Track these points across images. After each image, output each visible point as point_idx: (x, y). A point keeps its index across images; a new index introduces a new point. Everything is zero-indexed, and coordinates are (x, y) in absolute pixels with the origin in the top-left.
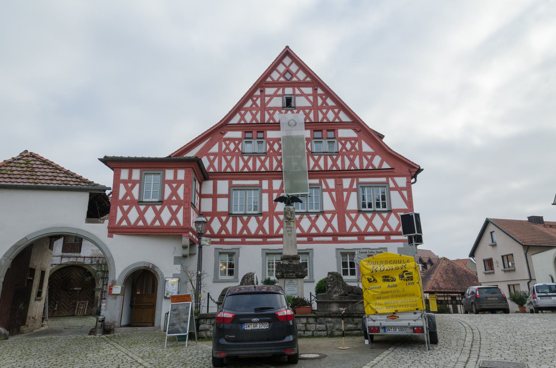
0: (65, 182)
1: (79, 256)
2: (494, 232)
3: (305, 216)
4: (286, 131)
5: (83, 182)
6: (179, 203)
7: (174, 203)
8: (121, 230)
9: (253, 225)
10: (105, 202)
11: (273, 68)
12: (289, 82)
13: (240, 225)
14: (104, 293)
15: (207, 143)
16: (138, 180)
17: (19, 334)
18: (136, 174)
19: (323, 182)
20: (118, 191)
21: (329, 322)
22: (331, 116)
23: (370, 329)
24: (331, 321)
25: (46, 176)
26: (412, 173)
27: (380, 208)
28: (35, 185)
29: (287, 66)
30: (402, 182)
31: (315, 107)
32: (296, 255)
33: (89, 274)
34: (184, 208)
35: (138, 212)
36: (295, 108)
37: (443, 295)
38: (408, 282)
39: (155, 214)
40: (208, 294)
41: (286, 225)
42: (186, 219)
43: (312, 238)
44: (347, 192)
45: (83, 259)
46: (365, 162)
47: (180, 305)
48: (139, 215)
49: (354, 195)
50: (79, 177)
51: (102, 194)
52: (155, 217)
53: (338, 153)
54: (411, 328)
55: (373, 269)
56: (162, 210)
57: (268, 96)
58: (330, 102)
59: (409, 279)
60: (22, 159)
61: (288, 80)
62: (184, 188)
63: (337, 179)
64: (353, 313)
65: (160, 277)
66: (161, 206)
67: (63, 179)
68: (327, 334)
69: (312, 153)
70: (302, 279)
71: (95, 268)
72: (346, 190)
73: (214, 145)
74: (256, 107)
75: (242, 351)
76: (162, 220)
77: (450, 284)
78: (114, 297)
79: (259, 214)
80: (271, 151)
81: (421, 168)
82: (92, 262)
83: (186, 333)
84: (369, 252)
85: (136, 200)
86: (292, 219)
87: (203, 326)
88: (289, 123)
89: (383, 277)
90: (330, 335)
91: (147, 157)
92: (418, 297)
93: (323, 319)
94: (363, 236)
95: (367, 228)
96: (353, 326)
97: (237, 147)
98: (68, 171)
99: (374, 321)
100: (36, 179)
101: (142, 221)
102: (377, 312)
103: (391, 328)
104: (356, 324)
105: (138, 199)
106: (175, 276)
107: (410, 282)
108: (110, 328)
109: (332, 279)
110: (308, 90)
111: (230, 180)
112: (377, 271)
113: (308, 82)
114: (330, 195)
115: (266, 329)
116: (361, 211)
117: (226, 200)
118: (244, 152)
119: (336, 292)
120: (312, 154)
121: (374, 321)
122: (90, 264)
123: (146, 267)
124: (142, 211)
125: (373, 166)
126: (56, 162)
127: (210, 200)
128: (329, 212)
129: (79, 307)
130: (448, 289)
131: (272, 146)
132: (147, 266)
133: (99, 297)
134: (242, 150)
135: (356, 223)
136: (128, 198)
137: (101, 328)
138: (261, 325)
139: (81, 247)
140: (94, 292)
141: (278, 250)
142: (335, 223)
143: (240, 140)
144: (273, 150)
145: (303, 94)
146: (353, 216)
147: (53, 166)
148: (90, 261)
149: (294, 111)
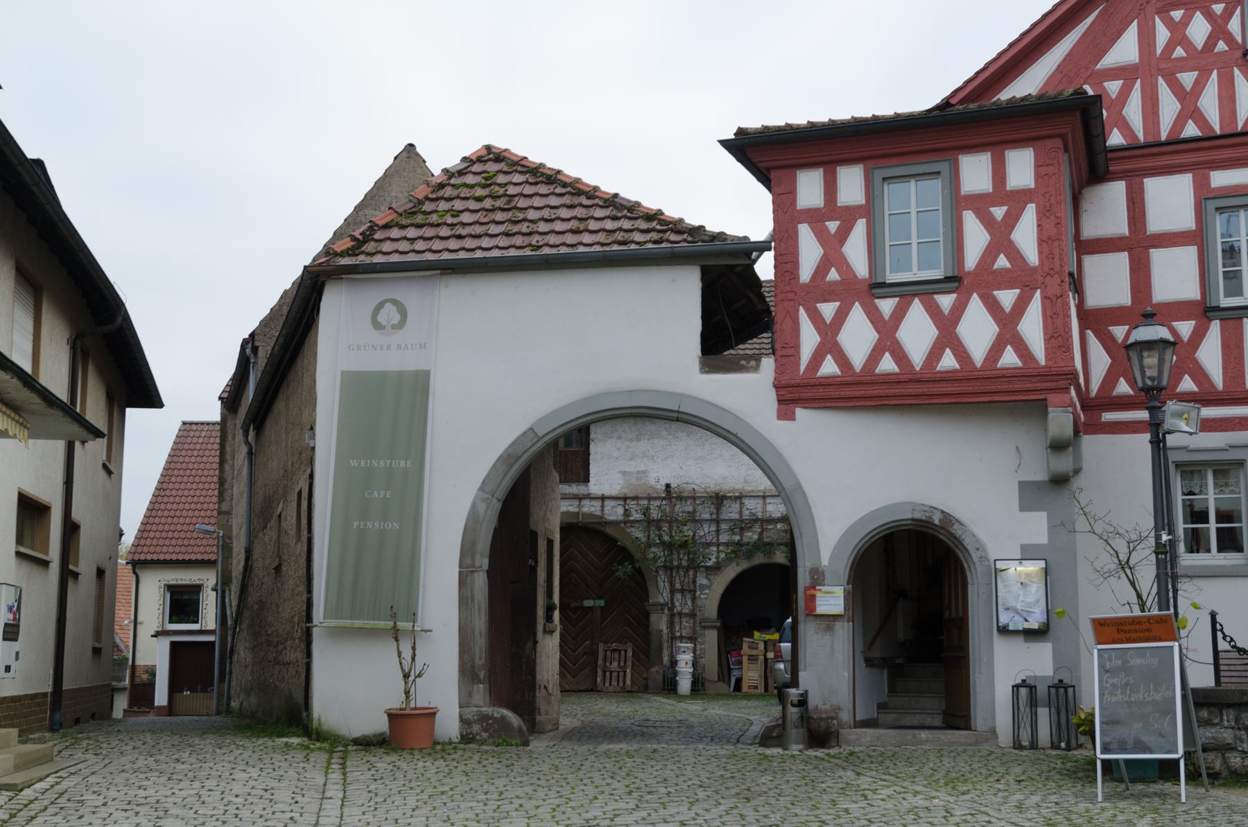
0: (619, 236)
1: (586, 493)
5: (672, 230)
6: (1023, 278)
7: (1005, 280)
8: (820, 392)
10: (751, 295)
14: (677, 619)
17: (534, 732)
25: (556, 222)
28: (534, 253)
33: (624, 554)
34: (1045, 298)
39: (938, 328)
40: (1213, 616)
45: (598, 504)
47: (1131, 652)
50: (655, 214)
51: (738, 269)
52: (937, 339)
56: (959, 309)
60: (470, 172)
62: (1039, 219)
65: (975, 556)
66: (955, 295)
67: (609, 225)
71: (638, 533)
73: (1119, 34)
76: (963, 346)
82: (627, 512)
85: (861, 280)
87: (1208, 734)
91: (782, 123)
98: (616, 195)
100: (530, 234)
105: (867, 276)
106: (1027, 554)
108: (828, 728)
111: (1201, 171)
117: (1189, 254)
122: (621, 522)
123: (922, 521)
126: (572, 170)
127: (1120, 262)
129: (607, 664)
132: (924, 518)
133: (665, 631)
136: (833, 275)
137: (802, 726)
139: (589, 464)
140: (647, 615)
147: (564, 185)
148: (620, 511)
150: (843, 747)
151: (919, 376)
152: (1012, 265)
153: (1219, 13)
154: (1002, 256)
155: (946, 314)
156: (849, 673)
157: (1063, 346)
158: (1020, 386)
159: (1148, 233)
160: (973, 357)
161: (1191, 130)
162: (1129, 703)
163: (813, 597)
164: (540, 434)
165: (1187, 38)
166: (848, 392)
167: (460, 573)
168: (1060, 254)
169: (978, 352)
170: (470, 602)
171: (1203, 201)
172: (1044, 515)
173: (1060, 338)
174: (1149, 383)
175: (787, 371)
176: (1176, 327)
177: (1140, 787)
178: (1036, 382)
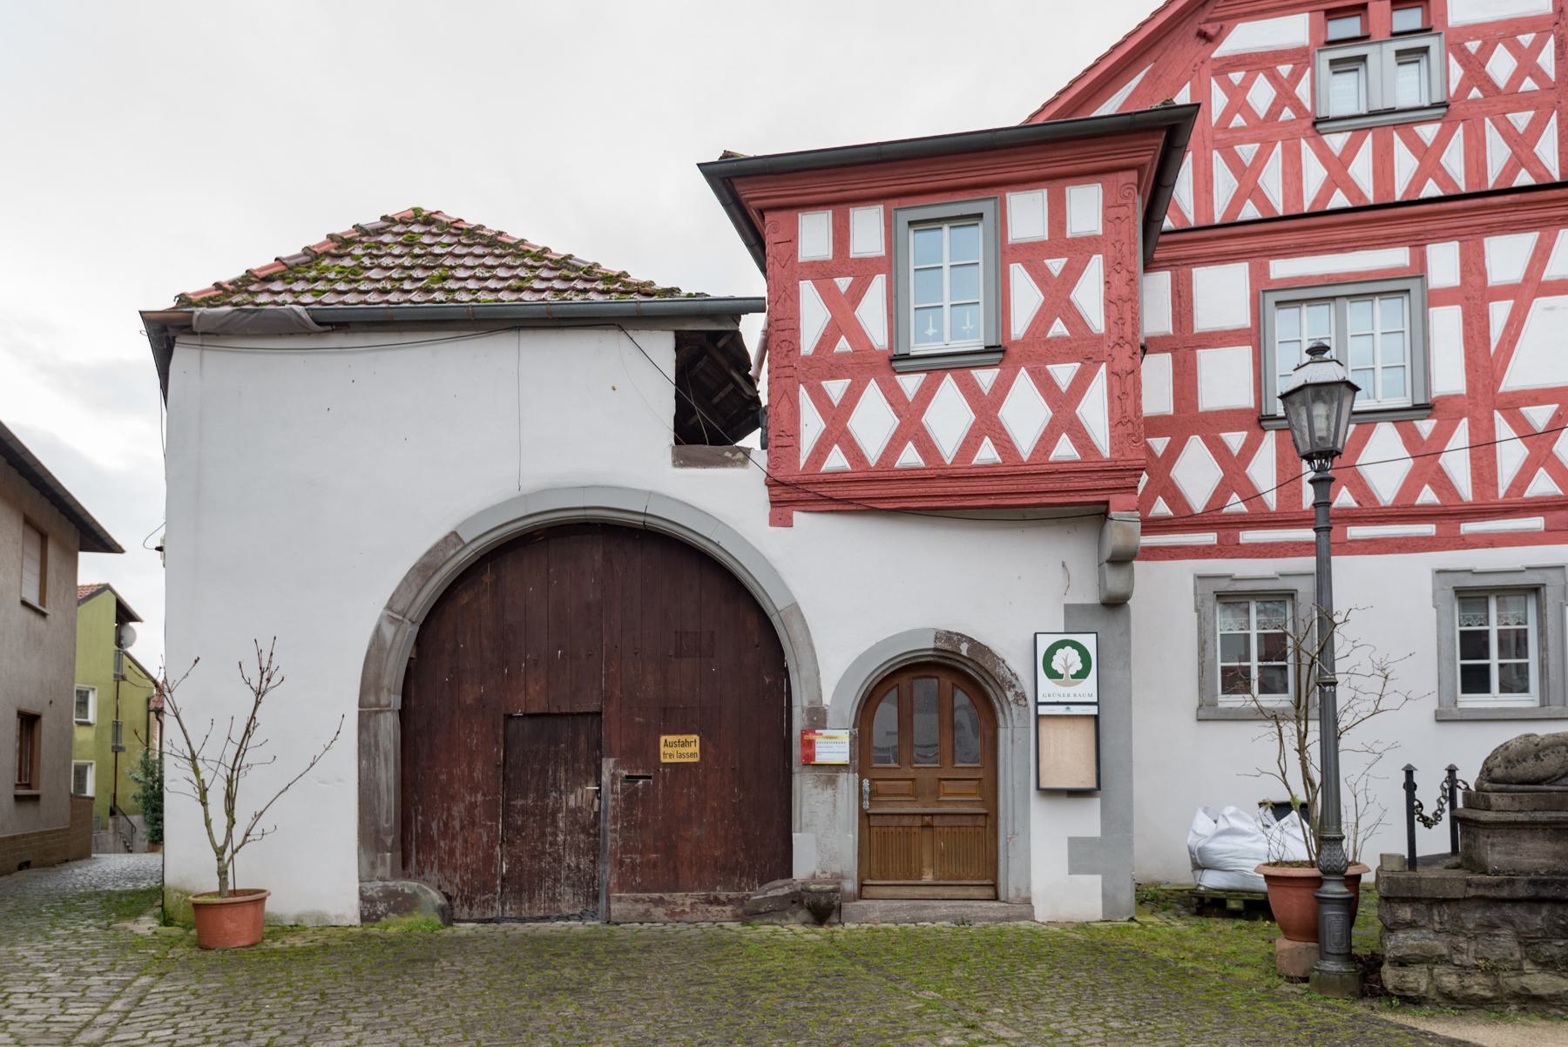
5: (639, 292)
6: (1085, 350)
7: (1060, 349)
20: (794, 317)
34: (1112, 373)
35: (892, 405)
39: (975, 411)
48: (898, 421)
56: (1002, 388)
62: (1107, 275)
66: (997, 371)
76: (1007, 435)
78: (824, 774)
80: (1475, 93)
97: (1285, 94)
105: (886, 346)
111: (1259, 260)
118: (1323, 114)
124: (910, 398)
126: (514, 231)
131: (1475, 68)
134: (1313, 104)
136: (843, 345)
141: (1521, 575)
143: (1300, 58)
144: (1487, 84)
150: (847, 925)
151: (950, 471)
152: (1071, 333)
154: (1058, 320)
155: (986, 394)
156: (854, 834)
157: (1134, 435)
158: (1077, 484)
159: (1196, 331)
160: (1019, 449)
164: (467, 540)
165: (1248, 104)
167: (360, 713)
168: (1133, 318)
169: (1025, 441)
170: (373, 749)
171: (1261, 294)
173: (1129, 425)
175: (783, 465)
176: (1225, 439)
178: (1097, 480)
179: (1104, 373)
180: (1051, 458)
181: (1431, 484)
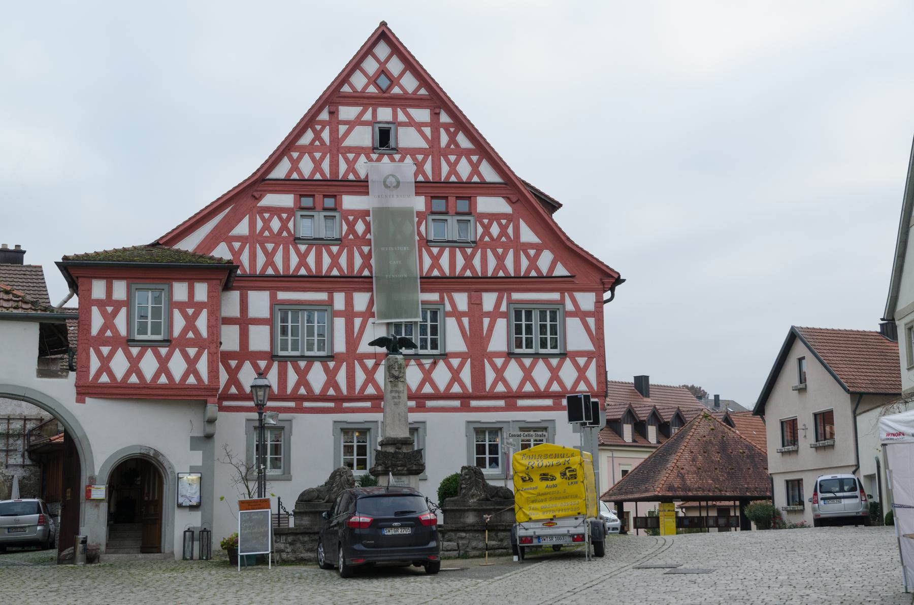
2: (804, 358)
3: (412, 362)
4: (379, 197)
5: (21, 301)
8: (99, 390)
9: (317, 377)
10: (61, 337)
11: (355, 65)
12: (386, 95)
13: (292, 378)
15: (226, 215)
16: (124, 301)
18: (120, 290)
19: (446, 298)
21: (462, 538)
22: (464, 169)
23: (521, 539)
24: (466, 536)
26: (606, 286)
27: (547, 348)
29: (382, 61)
30: (586, 300)
31: (434, 150)
32: (408, 438)
34: (209, 353)
35: (127, 358)
36: (396, 150)
37: (696, 504)
38: (570, 481)
40: (279, 499)
41: (390, 387)
42: (213, 372)
43: (425, 403)
44: (489, 319)
46: (525, 263)
47: (252, 514)
48: (129, 365)
49: (501, 324)
52: (158, 368)
53: (476, 243)
54: (570, 536)
55: (529, 464)
56: (169, 355)
57: (345, 123)
58: (463, 142)
59: (572, 478)
61: (384, 92)
62: (208, 317)
63: (473, 293)
64: (497, 526)
66: (168, 348)
68: (459, 555)
69: (427, 242)
70: (416, 476)
72: (488, 314)
74: (321, 145)
75: (383, 556)
76: (171, 373)
77: (710, 477)
79: (328, 357)
80: (351, 237)
81: (622, 278)
83: (268, 551)
84: (525, 435)
86: (400, 377)
88: (385, 182)
89: (541, 475)
90: (463, 555)
92: (582, 499)
93: (453, 534)
94: (515, 399)
95: (522, 384)
96: (497, 543)
97: (284, 227)
99: (527, 529)
101: (136, 375)
102: (530, 519)
103: (547, 538)
104: (501, 540)
106: (193, 470)
107: (572, 481)
109: (467, 477)
110: (422, 115)
111: (273, 291)
112: (533, 468)
113: (422, 97)
114: (458, 323)
115: (409, 534)
116: (513, 354)
117: (266, 329)
119: (474, 495)
120: (429, 244)
121: (527, 529)
123: (144, 454)
124: (135, 356)
125: (538, 270)
128: (456, 355)
130: (704, 491)
131: (351, 226)
132: (146, 453)
135: (503, 376)
136: (109, 333)
138: (403, 530)
142: (466, 375)
143: (290, 212)
144: (355, 233)
145: (411, 123)
146: (499, 362)
149: (394, 155)
151: (149, 386)
153: (285, 218)
154: (191, 332)
161: (270, 271)
162: (252, 533)
163: (90, 491)
166: (114, 391)
172: (201, 452)
174: (260, 402)
177: (250, 567)
179: (206, 354)
180: (187, 383)
181: (333, 387)
